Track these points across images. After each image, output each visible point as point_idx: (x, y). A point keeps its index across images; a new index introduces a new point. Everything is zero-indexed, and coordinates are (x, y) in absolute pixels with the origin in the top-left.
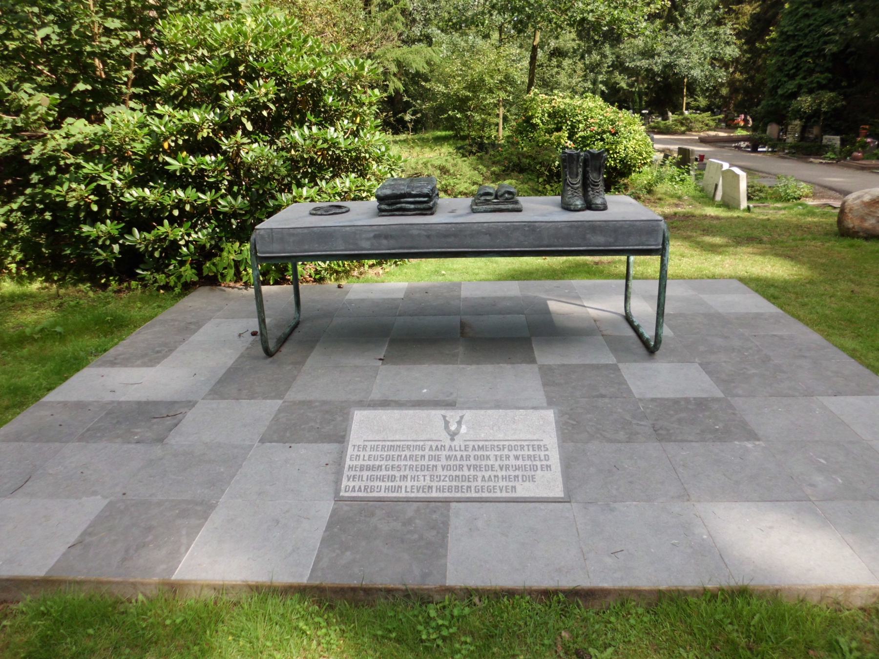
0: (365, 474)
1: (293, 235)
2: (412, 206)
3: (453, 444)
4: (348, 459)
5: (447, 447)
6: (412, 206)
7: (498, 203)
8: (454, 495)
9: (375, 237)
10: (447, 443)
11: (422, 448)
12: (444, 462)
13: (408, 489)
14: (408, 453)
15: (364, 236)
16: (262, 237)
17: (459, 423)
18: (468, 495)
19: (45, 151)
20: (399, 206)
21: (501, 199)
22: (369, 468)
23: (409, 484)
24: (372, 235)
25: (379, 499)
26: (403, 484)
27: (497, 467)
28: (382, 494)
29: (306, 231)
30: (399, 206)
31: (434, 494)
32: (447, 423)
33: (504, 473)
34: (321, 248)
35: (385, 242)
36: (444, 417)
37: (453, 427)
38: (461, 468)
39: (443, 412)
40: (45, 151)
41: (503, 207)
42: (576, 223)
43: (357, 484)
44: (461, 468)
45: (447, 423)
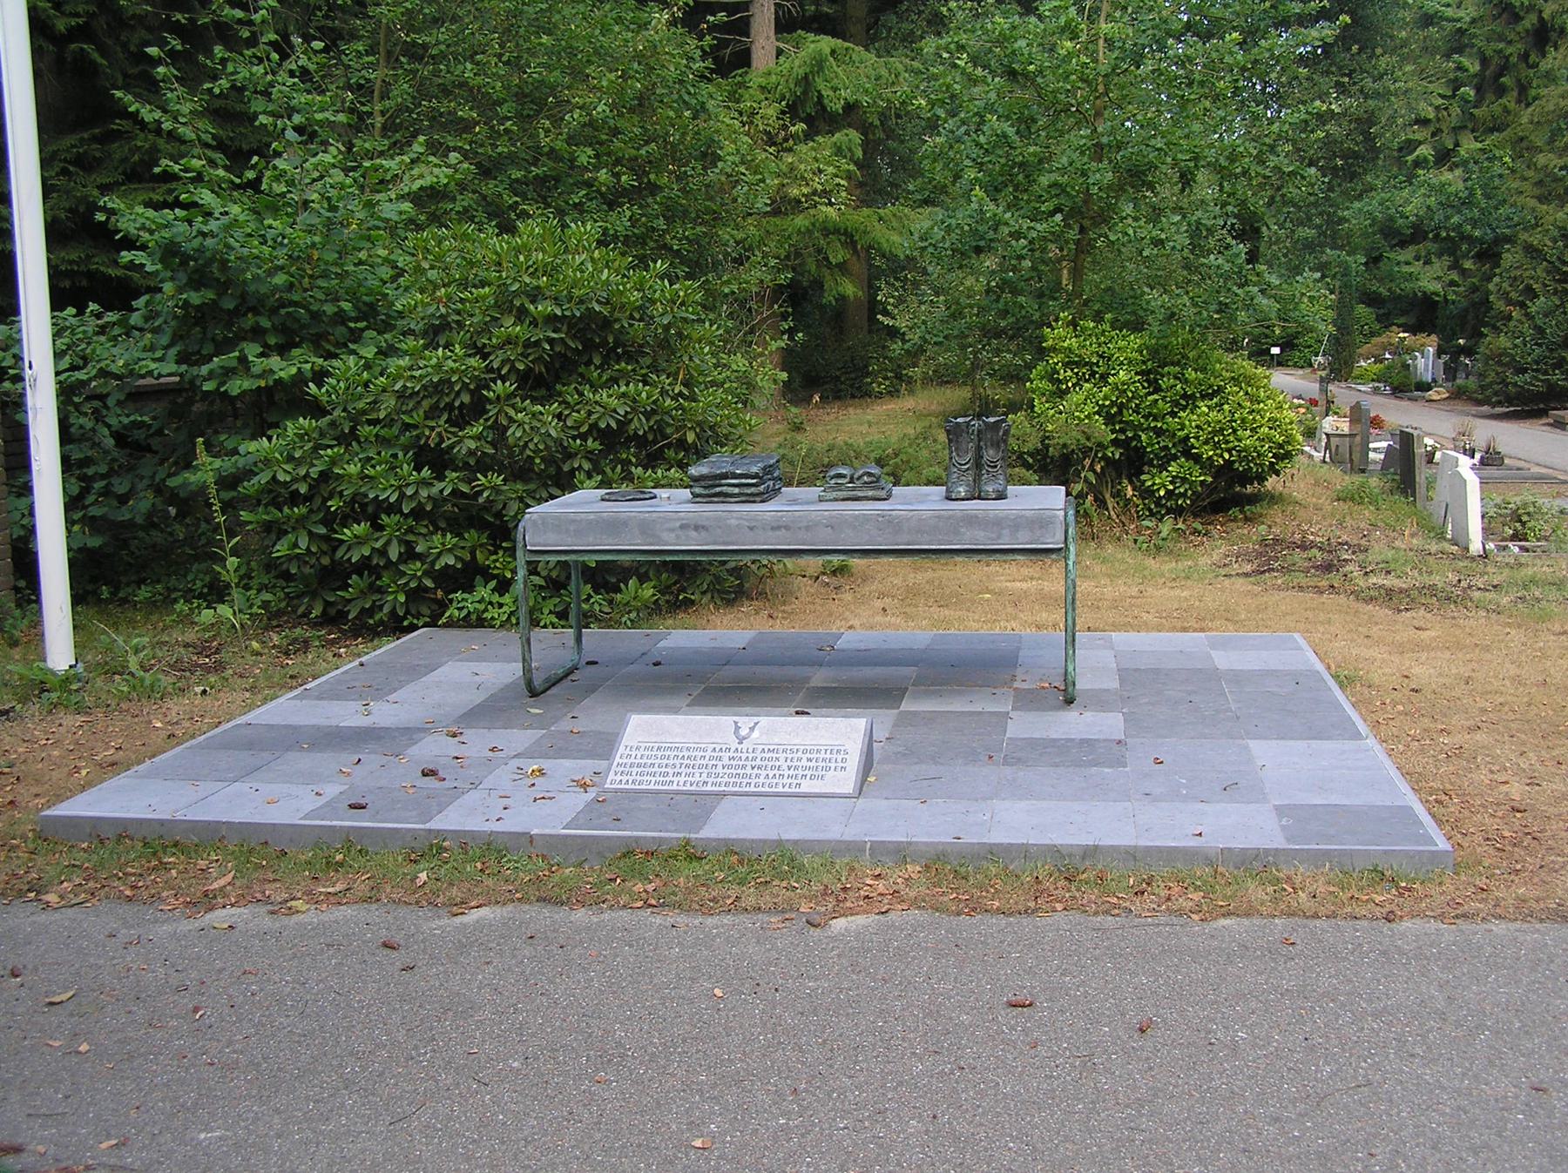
0: (635, 770)
1: (574, 521)
2: (736, 490)
3: (740, 747)
4: (618, 755)
5: (733, 749)
6: (736, 490)
7: (854, 489)
8: (731, 789)
9: (683, 527)
10: (734, 745)
11: (705, 750)
12: (726, 761)
13: (679, 783)
14: (686, 754)
15: (667, 526)
16: (534, 522)
17: (752, 729)
18: (747, 789)
19: (81, 375)
20: (718, 489)
21: (858, 483)
22: (639, 765)
23: (682, 779)
24: (678, 524)
25: (1010, 557)
26: (676, 779)
27: (785, 767)
28: (651, 787)
29: (592, 517)
30: (718, 489)
31: (709, 788)
32: (737, 728)
33: (791, 772)
34: (611, 541)
35: (693, 534)
36: (736, 723)
37: (744, 732)
38: (744, 767)
39: (736, 718)
40: (81, 375)
41: (860, 494)
42: (688, 558)
43: (625, 778)
44: (744, 767)
45: (737, 728)
